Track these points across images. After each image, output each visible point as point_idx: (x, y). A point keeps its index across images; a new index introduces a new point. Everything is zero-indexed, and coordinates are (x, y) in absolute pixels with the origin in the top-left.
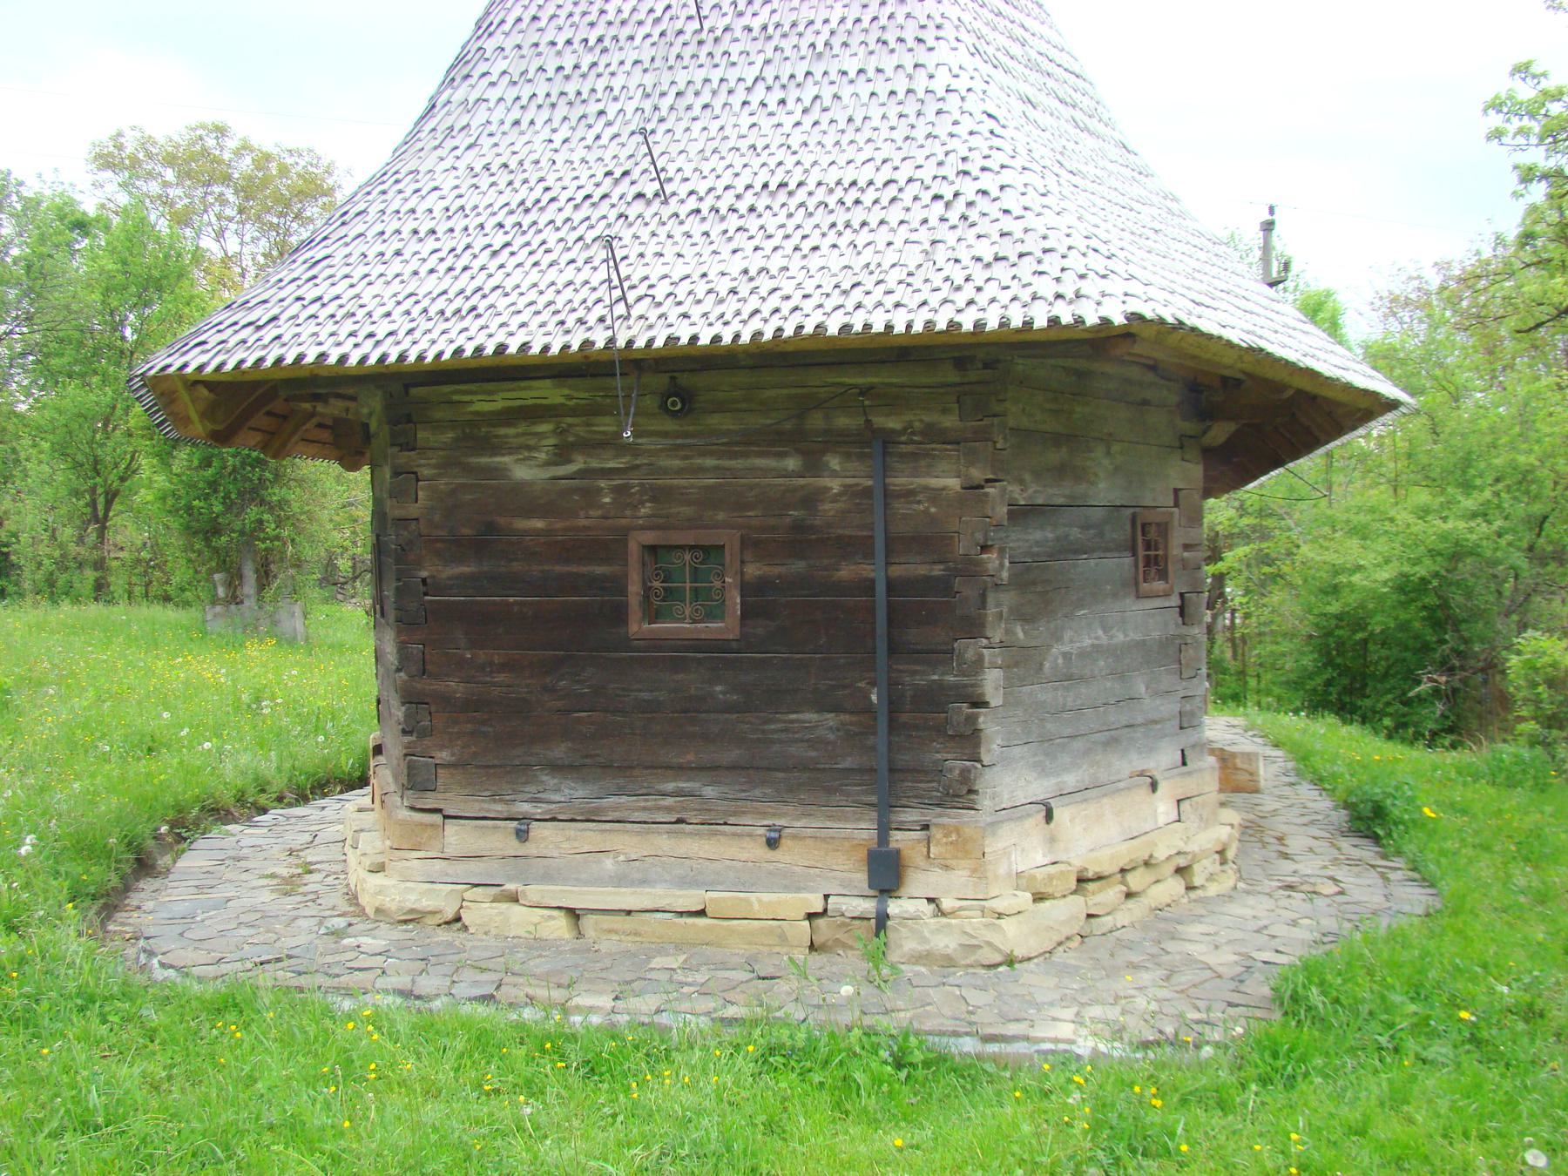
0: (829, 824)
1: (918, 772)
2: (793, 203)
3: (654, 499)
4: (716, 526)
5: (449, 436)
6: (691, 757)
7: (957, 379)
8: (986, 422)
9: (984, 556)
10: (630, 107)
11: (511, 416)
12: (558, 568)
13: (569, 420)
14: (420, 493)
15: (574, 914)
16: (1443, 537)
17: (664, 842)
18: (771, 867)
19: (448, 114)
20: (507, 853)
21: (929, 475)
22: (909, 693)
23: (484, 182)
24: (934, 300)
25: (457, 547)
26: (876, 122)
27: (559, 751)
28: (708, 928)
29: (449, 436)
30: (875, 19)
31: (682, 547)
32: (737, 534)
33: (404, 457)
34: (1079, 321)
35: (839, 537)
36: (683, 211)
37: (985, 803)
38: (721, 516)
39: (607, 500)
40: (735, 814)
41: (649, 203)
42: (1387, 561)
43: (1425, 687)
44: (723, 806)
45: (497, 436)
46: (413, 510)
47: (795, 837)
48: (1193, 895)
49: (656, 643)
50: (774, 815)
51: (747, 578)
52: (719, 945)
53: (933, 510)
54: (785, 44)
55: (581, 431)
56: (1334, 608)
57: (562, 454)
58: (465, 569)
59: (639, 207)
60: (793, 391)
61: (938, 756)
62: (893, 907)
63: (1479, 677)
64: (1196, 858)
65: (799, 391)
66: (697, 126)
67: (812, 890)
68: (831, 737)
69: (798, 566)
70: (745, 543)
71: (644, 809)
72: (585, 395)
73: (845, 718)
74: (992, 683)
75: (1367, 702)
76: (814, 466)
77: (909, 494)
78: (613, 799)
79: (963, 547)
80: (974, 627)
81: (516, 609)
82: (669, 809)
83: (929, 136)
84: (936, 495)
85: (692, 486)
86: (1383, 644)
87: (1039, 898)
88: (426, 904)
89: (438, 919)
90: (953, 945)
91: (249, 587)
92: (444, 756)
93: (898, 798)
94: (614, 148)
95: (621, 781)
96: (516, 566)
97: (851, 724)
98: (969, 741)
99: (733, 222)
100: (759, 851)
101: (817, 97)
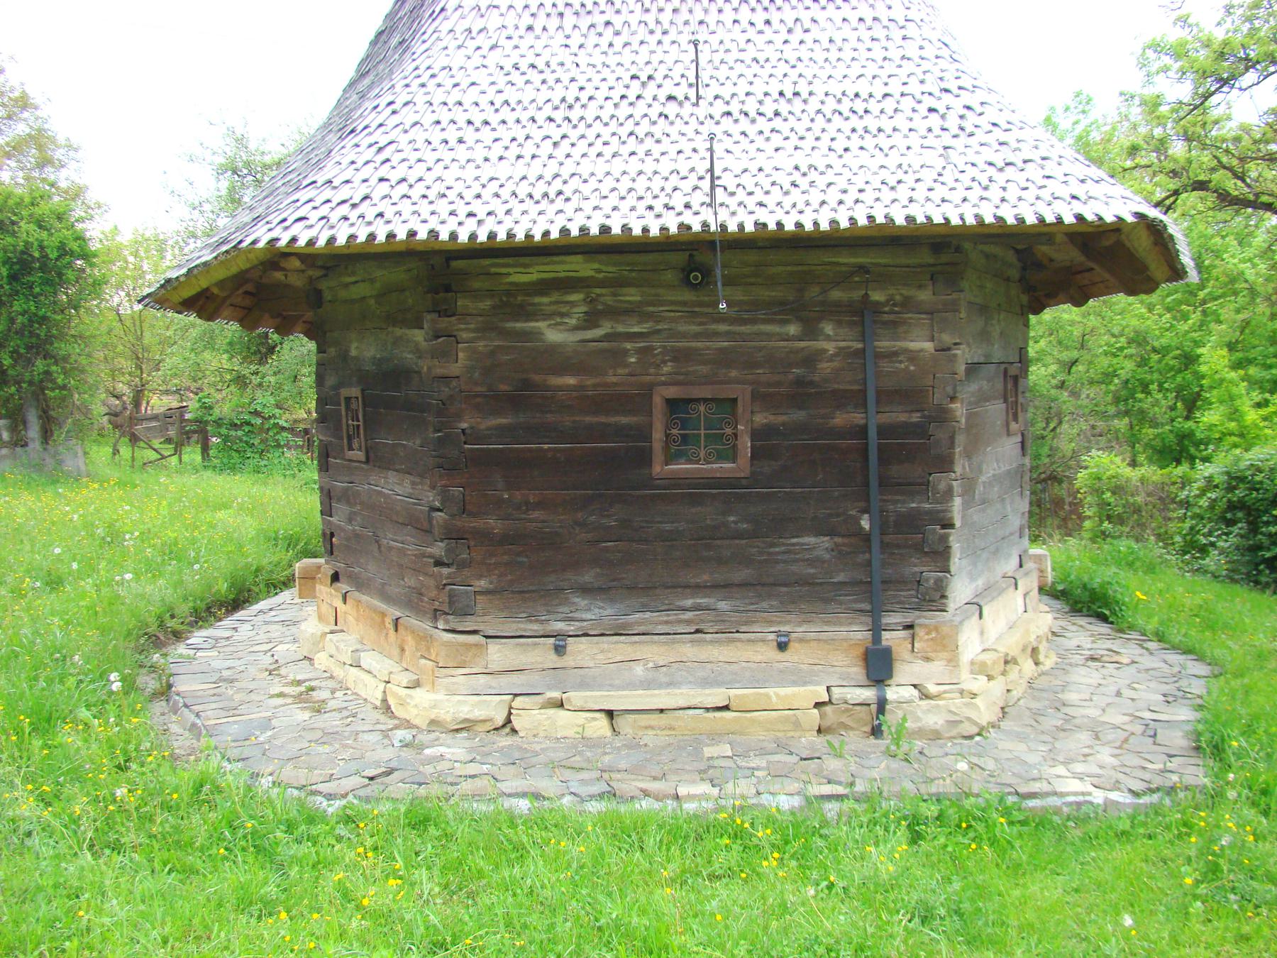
0: (826, 628)
1: (899, 582)
3: (674, 359)
4: (729, 382)
5: (486, 304)
6: (706, 577)
7: (931, 261)
8: (955, 296)
9: (953, 406)
10: (634, 20)
11: (545, 287)
12: (589, 419)
13: (598, 291)
14: (461, 355)
15: (610, 714)
17: (688, 650)
18: (781, 666)
20: (546, 666)
21: (905, 339)
22: (892, 519)
25: (495, 402)
27: (588, 577)
28: (735, 720)
29: (486, 304)
31: (697, 400)
32: (749, 388)
33: (444, 323)
35: (834, 392)
38: (734, 373)
39: (633, 360)
40: (746, 623)
44: (735, 617)
45: (534, 304)
46: (455, 369)
47: (801, 640)
49: (677, 481)
50: (780, 623)
51: (755, 425)
52: (742, 734)
53: (912, 368)
55: (609, 300)
57: (591, 320)
58: (503, 421)
59: (671, 109)
60: (795, 269)
61: (916, 569)
65: (800, 268)
67: (818, 684)
68: (827, 556)
69: (799, 416)
70: (755, 396)
71: (667, 622)
72: (610, 269)
73: (838, 540)
76: (811, 331)
77: (893, 355)
78: (638, 615)
79: (938, 398)
80: (945, 464)
81: (550, 455)
82: (688, 622)
84: (913, 356)
85: (708, 348)
88: (478, 714)
89: (489, 726)
90: (941, 722)
91: (34, 432)
92: (483, 584)
93: (885, 604)
94: (627, 57)
95: (644, 600)
96: (550, 418)
97: (844, 545)
98: (941, 556)
99: (762, 123)
100: (772, 653)
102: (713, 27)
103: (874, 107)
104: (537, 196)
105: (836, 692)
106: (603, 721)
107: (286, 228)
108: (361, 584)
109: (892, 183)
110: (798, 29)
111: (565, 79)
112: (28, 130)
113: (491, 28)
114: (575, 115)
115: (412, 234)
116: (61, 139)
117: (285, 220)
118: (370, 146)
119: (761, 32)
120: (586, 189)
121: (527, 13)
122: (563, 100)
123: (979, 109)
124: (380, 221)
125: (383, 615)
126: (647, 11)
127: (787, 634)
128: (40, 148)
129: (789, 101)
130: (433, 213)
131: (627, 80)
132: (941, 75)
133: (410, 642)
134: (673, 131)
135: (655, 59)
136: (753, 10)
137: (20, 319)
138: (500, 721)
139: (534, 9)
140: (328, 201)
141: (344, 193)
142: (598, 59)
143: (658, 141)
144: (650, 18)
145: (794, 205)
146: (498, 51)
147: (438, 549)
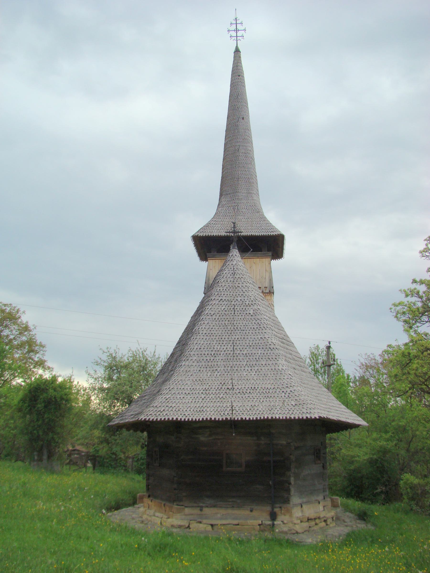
2: (257, 391)
10: (222, 369)
15: (212, 525)
16: (381, 447)
17: (230, 511)
19: (185, 367)
23: (196, 383)
24: (286, 412)
26: (269, 375)
30: (267, 353)
34: (311, 417)
36: (237, 392)
37: (291, 503)
41: (230, 390)
42: (366, 454)
43: (379, 490)
48: (327, 526)
54: (250, 358)
56: (352, 467)
59: (228, 391)
62: (275, 523)
63: (394, 488)
64: (328, 518)
66: (236, 374)
74: (292, 480)
75: (363, 495)
80: (289, 469)
83: (280, 379)
86: (367, 478)
87: (301, 522)
91: (45, 457)
92: (184, 494)
98: (288, 491)
101: (258, 369)
102: (239, 371)
103: (271, 391)
104: (198, 411)
105: (263, 522)
106: (210, 527)
107: (148, 416)
108: (155, 497)
109: (270, 409)
110: (258, 372)
111: (206, 383)
112: (26, 339)
113: (191, 370)
114: (207, 392)
115: (173, 418)
116: (38, 342)
117: (147, 414)
118: (165, 398)
119: (249, 372)
120: (208, 409)
121: (199, 367)
122: (205, 388)
123: (293, 391)
124: (166, 416)
125: (161, 503)
126: (225, 367)
127: (253, 508)
128: (30, 346)
129: (253, 390)
130: (177, 414)
131: (219, 383)
132: (287, 383)
133: (168, 509)
134: (227, 396)
135: (226, 378)
136: (248, 367)
137: (46, 420)
138: (187, 525)
139: (201, 366)
140: (156, 411)
141: (159, 409)
142: (214, 379)
143: (224, 399)
144: (226, 369)
145: (249, 414)
146: (192, 376)
147: (175, 486)
